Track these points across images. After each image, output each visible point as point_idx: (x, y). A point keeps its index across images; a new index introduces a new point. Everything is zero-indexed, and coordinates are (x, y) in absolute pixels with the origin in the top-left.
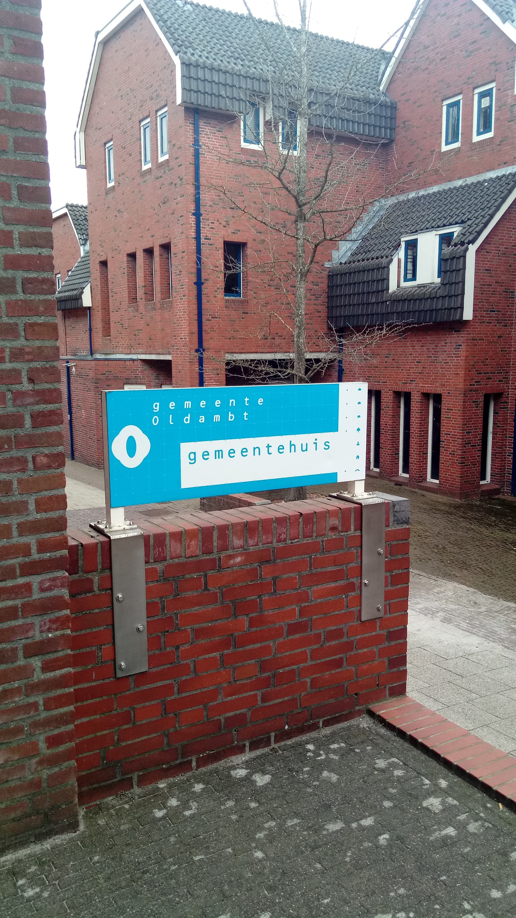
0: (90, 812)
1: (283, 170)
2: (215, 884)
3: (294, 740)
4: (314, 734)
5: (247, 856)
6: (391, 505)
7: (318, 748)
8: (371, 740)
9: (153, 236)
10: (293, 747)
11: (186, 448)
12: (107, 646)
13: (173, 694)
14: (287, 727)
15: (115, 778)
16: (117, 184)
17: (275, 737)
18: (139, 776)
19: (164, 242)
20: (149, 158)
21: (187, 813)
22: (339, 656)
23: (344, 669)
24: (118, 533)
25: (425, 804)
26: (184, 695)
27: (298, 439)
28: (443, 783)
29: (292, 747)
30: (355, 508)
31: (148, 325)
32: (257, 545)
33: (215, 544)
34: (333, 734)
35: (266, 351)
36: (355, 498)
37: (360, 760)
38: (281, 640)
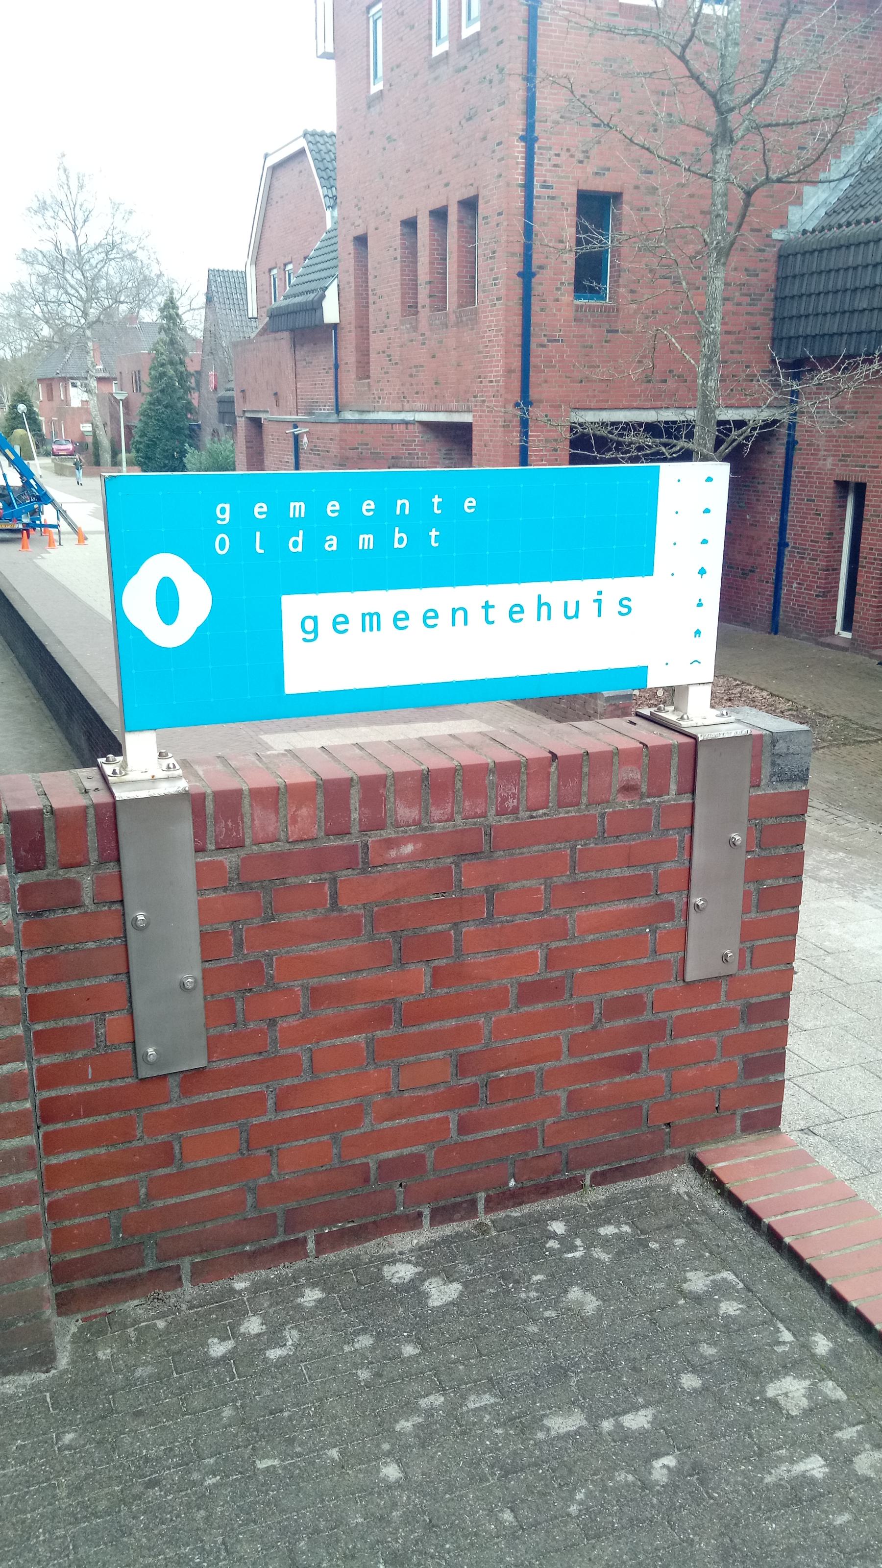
0: (89, 1330)
1: (690, 40)
2: (283, 1531)
3: (526, 1209)
4: (571, 1200)
5: (366, 1471)
6: (768, 740)
7: (573, 1232)
8: (688, 1224)
9: (447, 185)
10: (521, 1225)
11: (294, 607)
12: (116, 1016)
13: (265, 1113)
14: (512, 1183)
15: (143, 1265)
16: (388, 86)
17: (488, 1199)
18: (193, 1265)
19: (466, 197)
20: (444, 32)
21: (273, 1354)
22: (631, 1050)
23: (642, 1076)
24: (128, 786)
25: (771, 1391)
26: (288, 1115)
27: (557, 592)
28: (822, 1345)
29: (520, 1223)
30: (680, 745)
31: (434, 357)
32: (451, 819)
33: (355, 816)
34: (611, 1202)
35: (649, 404)
36: (684, 724)
37: (656, 1269)
38: (504, 1013)
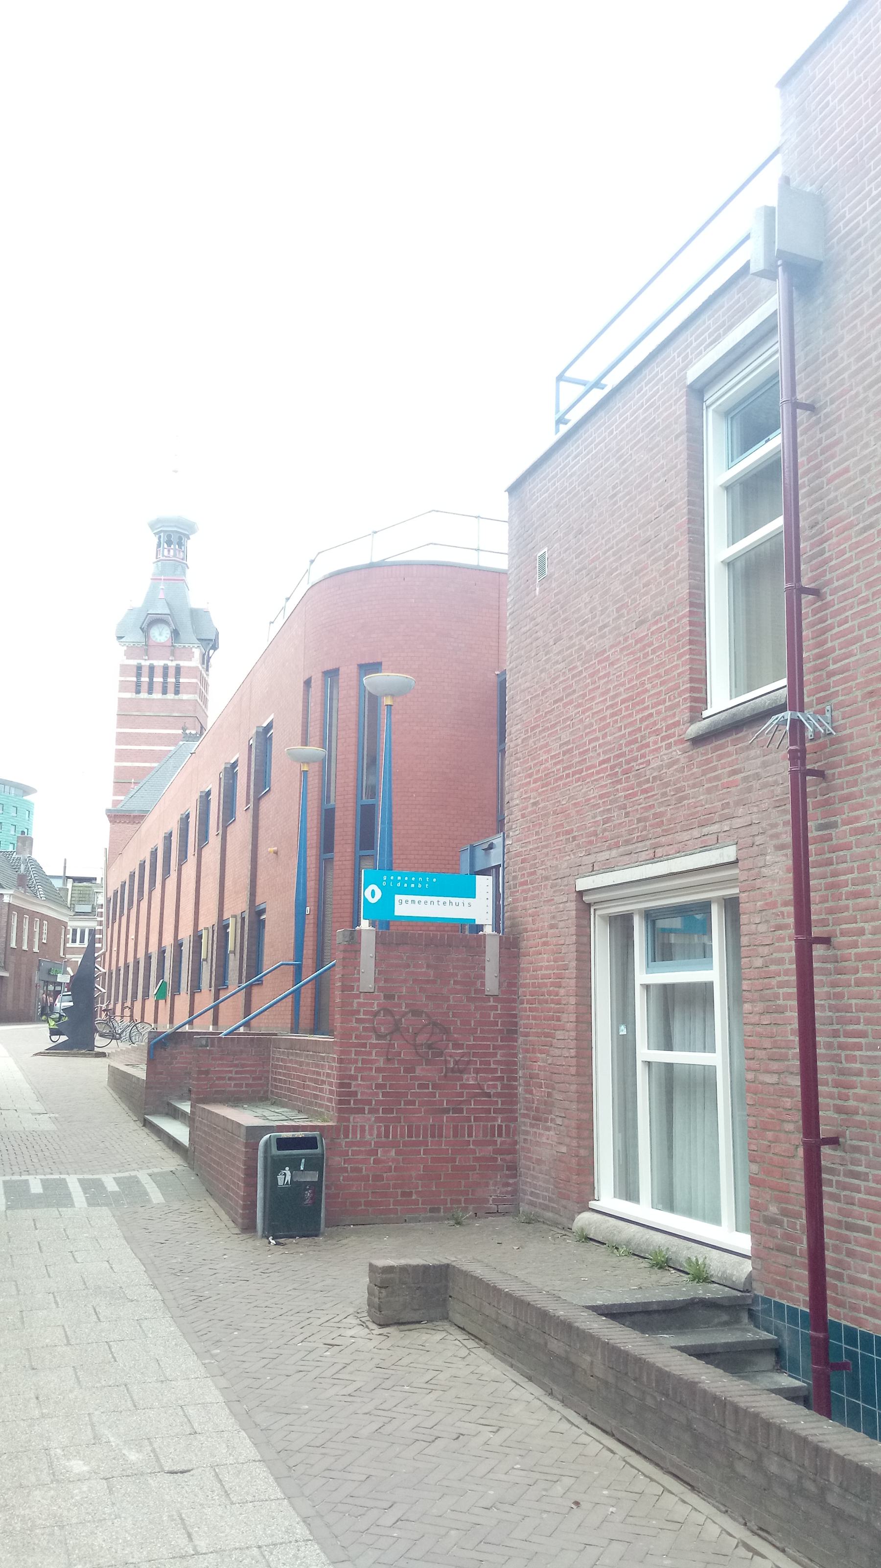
11: (397, 897)
